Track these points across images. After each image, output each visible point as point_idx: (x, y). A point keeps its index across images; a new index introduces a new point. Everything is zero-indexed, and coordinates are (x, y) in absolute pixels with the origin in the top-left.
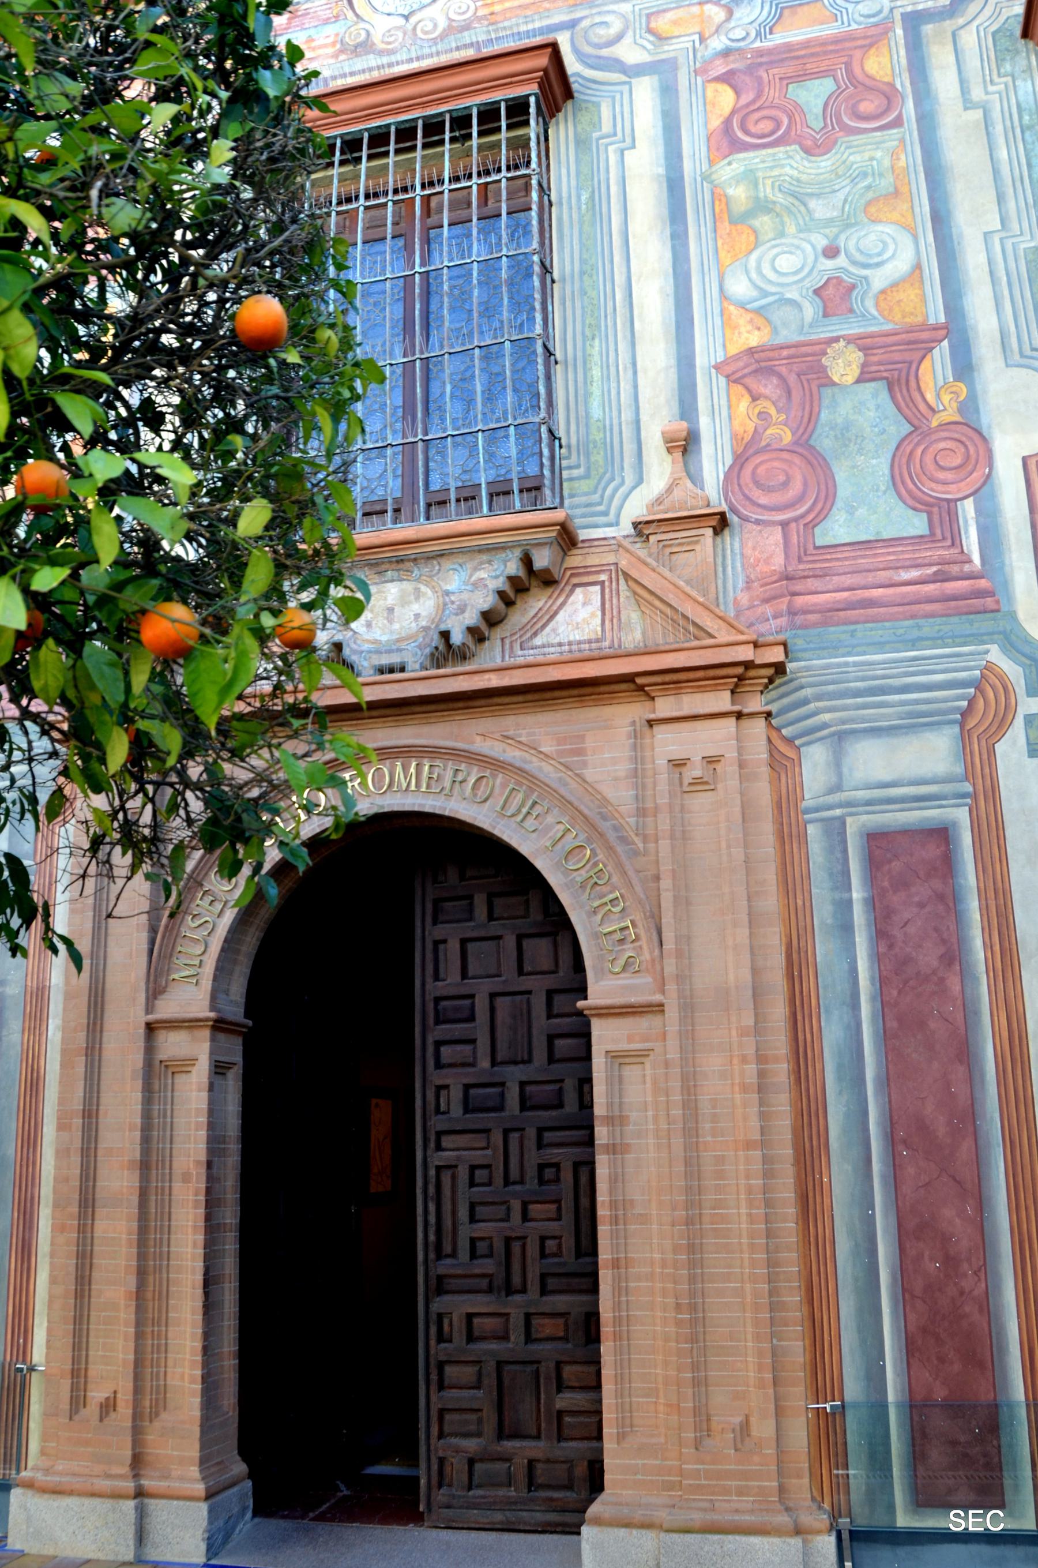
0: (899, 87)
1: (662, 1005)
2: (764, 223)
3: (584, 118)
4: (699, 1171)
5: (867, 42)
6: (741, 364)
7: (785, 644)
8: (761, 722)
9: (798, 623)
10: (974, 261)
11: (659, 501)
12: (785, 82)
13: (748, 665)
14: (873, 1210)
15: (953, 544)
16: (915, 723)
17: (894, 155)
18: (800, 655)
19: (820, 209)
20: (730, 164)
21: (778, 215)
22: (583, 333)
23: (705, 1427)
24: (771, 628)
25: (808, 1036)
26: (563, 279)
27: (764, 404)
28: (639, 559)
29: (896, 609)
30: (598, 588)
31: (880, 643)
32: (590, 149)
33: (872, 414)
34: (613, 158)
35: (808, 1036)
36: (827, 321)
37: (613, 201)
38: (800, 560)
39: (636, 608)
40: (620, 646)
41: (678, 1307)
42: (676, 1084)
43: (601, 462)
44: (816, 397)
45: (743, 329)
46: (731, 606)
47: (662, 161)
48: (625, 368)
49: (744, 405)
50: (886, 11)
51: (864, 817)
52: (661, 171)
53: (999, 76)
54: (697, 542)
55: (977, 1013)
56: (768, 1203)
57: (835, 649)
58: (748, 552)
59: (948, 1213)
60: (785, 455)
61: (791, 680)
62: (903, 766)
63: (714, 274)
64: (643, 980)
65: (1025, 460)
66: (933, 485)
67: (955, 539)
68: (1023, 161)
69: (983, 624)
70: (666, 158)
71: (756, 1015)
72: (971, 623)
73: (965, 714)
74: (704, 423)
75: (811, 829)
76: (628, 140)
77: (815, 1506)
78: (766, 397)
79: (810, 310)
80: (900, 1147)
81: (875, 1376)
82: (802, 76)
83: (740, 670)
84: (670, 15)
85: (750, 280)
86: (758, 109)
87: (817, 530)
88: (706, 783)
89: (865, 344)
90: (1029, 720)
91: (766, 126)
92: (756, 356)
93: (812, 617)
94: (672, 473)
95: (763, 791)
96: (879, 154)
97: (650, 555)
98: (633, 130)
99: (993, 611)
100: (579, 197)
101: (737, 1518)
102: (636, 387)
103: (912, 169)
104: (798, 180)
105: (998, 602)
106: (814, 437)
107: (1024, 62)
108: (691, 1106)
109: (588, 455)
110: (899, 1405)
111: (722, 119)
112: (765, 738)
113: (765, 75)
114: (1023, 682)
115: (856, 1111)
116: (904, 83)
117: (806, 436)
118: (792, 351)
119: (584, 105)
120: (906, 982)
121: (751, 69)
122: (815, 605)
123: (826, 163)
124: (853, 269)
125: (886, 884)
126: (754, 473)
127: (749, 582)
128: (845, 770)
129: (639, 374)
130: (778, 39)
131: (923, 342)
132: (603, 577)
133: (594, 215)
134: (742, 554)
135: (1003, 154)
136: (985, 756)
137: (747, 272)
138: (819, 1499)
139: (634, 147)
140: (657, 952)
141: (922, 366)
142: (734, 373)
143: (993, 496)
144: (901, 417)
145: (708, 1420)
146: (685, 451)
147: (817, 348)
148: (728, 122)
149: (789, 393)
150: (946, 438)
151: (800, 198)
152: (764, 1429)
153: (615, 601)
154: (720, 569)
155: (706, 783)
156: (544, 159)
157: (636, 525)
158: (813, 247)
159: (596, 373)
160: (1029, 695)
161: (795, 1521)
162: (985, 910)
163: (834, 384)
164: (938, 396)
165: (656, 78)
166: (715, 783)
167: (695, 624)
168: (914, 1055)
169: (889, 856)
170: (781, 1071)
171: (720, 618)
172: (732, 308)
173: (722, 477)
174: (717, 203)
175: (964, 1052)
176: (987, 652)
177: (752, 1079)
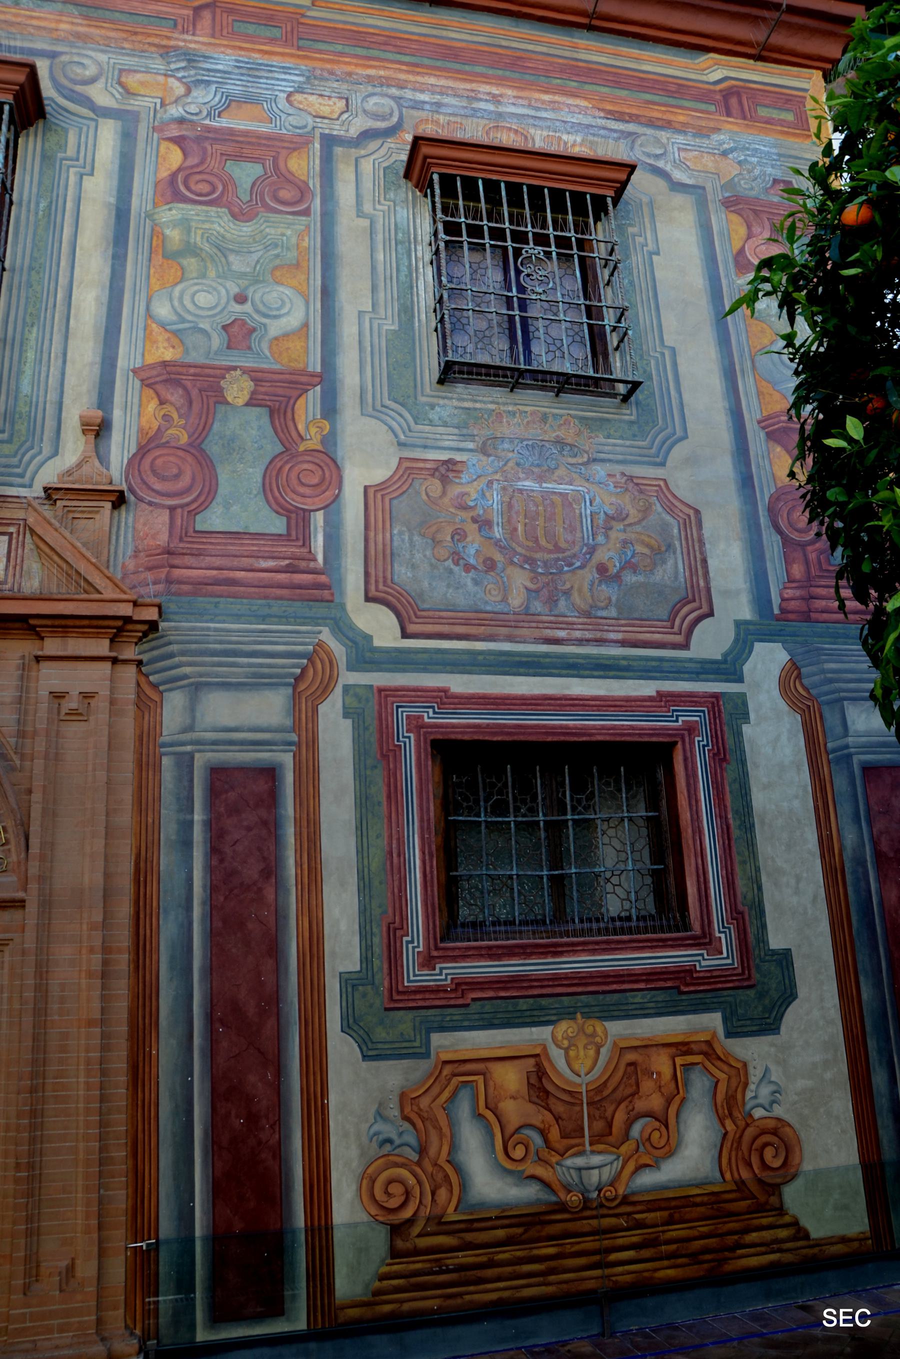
0: (311, 186)
1: (24, 901)
2: (191, 263)
3: (53, 138)
4: (45, 1046)
5: (292, 146)
6: (154, 372)
7: (159, 607)
8: (132, 669)
9: (173, 590)
10: (348, 331)
11: (69, 473)
12: (225, 158)
13: (128, 620)
14: (192, 1077)
15: (304, 545)
16: (258, 682)
17: (300, 236)
18: (172, 617)
19: (237, 264)
20: (170, 209)
21: (203, 260)
22: (24, 319)
23: (34, 1272)
24: (150, 592)
25: (148, 931)
26: (13, 270)
27: (168, 408)
28: (45, 518)
29: (253, 590)
30: (6, 538)
31: (237, 615)
32: (54, 166)
33: (254, 432)
34: (72, 179)
35: (148, 931)
36: (229, 352)
37: (67, 214)
38: (181, 540)
39: (37, 559)
40: (19, 591)
41: (18, 1166)
42: (30, 970)
43: (24, 432)
44: (211, 411)
45: (160, 345)
46: (119, 568)
47: (115, 193)
48: (56, 357)
49: (152, 406)
50: (309, 128)
51: (210, 754)
52: (113, 200)
53: (385, 199)
54: (97, 512)
55: (286, 917)
56: (104, 1073)
57: (200, 615)
58: (139, 527)
59: (252, 1078)
60: (180, 453)
61: (162, 637)
62: (242, 716)
63: (144, 295)
64: (10, 879)
65: (366, 488)
66: (295, 496)
67: (306, 541)
68: (394, 265)
69: (320, 610)
70: (119, 191)
71: (105, 913)
72: (310, 608)
73: (298, 679)
74: (117, 415)
75: (165, 761)
76: (88, 167)
77: (127, 1333)
78: (171, 403)
79: (217, 341)
80: (217, 1025)
81: (186, 1217)
82: (239, 157)
83: (119, 623)
84: (139, 76)
85: (173, 306)
86: (199, 173)
87: (198, 518)
88: (81, 714)
89: (257, 376)
90: (346, 689)
91: (204, 188)
92: (168, 369)
93: (185, 588)
94: (84, 451)
95: (128, 726)
96: (289, 232)
97: (55, 517)
98: (93, 160)
99: (328, 601)
100: (38, 204)
101: (56, 1354)
102: (63, 374)
103: (312, 250)
104: (223, 237)
105: (332, 594)
106: (206, 442)
107: (404, 195)
108: (42, 990)
109: (13, 424)
110: (204, 1239)
111: (169, 172)
112: (134, 681)
113: (209, 148)
114: (344, 659)
115: (183, 996)
116: (315, 184)
117: (198, 441)
118: (198, 370)
119: (54, 127)
120: (231, 891)
121: (199, 140)
122: (189, 577)
123: (247, 229)
124: (256, 316)
125: (222, 810)
126: (155, 459)
127: (137, 552)
128: (198, 715)
129: (68, 364)
130: (224, 122)
131: (302, 384)
132: (12, 529)
133: (49, 222)
134: (134, 528)
135: (380, 257)
136: (310, 714)
137: (171, 300)
138: (132, 1326)
139: (92, 174)
140: (23, 855)
141: (298, 402)
142: (148, 379)
143: (339, 512)
144: (276, 439)
145: (38, 1266)
146: (97, 435)
147: (218, 372)
148: (174, 176)
149: (191, 403)
150: (309, 462)
151: (223, 251)
152: (87, 1270)
153: (20, 551)
154: (114, 537)
155: (81, 714)
156: (10, 162)
157: (46, 490)
158: (227, 291)
159: (30, 355)
160: (348, 670)
161: (109, 1350)
162: (298, 835)
163: (228, 403)
164: (307, 428)
165: (119, 123)
166: (88, 715)
167: (86, 580)
168: (234, 950)
169: (226, 787)
170: (123, 961)
171: (108, 578)
172: (154, 325)
173: (125, 461)
174: (155, 238)
175: (274, 948)
176: (320, 632)
177: (97, 967)
